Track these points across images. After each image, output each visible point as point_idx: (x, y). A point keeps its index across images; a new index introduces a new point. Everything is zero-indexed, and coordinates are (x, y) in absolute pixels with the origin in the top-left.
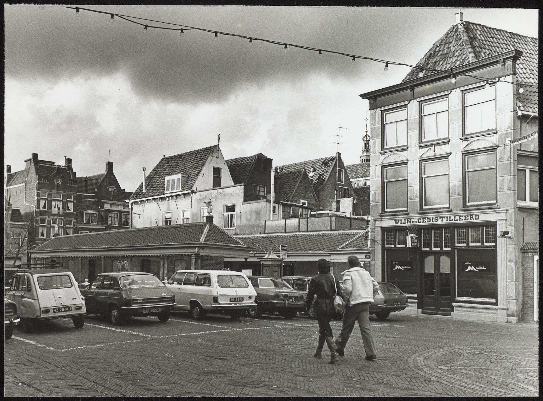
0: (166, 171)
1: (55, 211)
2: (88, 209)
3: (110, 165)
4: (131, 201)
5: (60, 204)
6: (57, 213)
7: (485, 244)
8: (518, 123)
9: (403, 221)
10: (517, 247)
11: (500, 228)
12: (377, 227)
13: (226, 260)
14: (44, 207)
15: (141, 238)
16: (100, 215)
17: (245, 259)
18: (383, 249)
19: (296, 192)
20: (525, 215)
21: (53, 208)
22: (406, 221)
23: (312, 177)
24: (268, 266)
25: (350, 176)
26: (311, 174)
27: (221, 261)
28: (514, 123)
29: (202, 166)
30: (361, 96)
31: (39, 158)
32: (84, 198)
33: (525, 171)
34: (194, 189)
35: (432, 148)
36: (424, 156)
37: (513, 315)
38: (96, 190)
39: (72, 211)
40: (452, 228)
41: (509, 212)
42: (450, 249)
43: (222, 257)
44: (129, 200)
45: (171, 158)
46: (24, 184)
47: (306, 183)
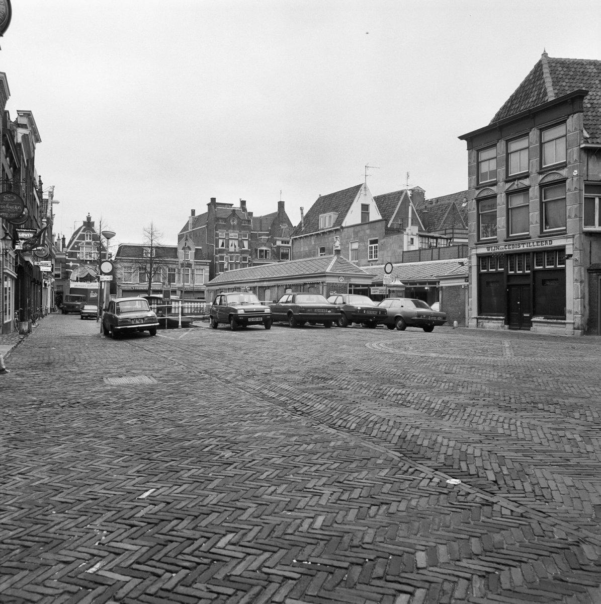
1: (232, 249)
3: (281, 205)
5: (236, 243)
8: (584, 156)
9: (493, 248)
10: (583, 268)
11: (568, 252)
14: (223, 245)
15: (286, 270)
16: (273, 252)
19: (444, 223)
20: (591, 239)
21: (230, 247)
28: (580, 156)
29: (351, 204)
30: (459, 138)
31: (217, 201)
33: (594, 198)
34: (343, 225)
35: (516, 182)
36: (510, 189)
37: (578, 329)
38: (270, 228)
39: (246, 248)
40: (531, 254)
41: (576, 237)
42: (503, 269)
45: (326, 197)
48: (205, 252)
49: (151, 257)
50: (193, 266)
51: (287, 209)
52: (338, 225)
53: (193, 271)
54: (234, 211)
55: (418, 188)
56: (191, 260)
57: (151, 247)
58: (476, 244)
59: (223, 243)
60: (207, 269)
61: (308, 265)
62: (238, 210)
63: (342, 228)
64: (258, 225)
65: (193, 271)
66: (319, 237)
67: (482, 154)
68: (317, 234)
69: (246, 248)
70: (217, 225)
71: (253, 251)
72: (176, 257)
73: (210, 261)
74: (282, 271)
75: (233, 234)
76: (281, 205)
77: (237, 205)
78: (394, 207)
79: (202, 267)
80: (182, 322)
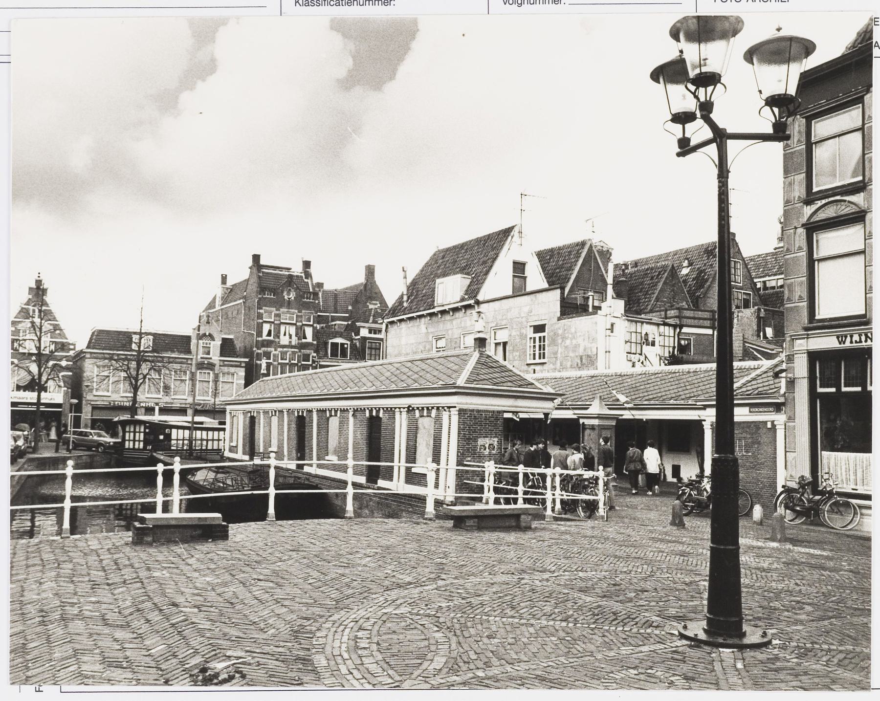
0: (439, 272)
1: (284, 340)
2: (335, 337)
3: (370, 271)
4: (386, 321)
5: (293, 330)
6: (287, 343)
7: (844, 389)
9: (856, 338)
12: (799, 352)
13: (506, 415)
14: (269, 334)
15: (371, 378)
16: (353, 346)
17: (544, 414)
18: (813, 395)
19: (657, 300)
22: (863, 338)
23: (687, 275)
24: (593, 428)
25: (754, 274)
26: (685, 271)
27: (497, 419)
31: (262, 262)
32: (332, 321)
34: (480, 297)
38: (350, 308)
43: (499, 412)
44: (383, 319)
46: (241, 301)
47: (673, 285)
48: (238, 345)
49: (139, 351)
50: (217, 368)
51: (380, 280)
52: (470, 298)
53: (216, 376)
54: (291, 276)
55: (602, 244)
56: (215, 357)
57: (140, 334)
58: (806, 329)
59: (270, 332)
60: (242, 372)
61: (417, 369)
62: (297, 276)
63: (478, 303)
64: (331, 302)
65: (216, 376)
66: (434, 318)
67: (818, 125)
68: (432, 315)
69: (309, 338)
70: (260, 299)
71: (320, 346)
72: (189, 352)
73: (247, 360)
74: (364, 380)
75: (288, 315)
76: (370, 271)
77: (297, 269)
78: (571, 269)
79: (232, 370)
80: (154, 485)
